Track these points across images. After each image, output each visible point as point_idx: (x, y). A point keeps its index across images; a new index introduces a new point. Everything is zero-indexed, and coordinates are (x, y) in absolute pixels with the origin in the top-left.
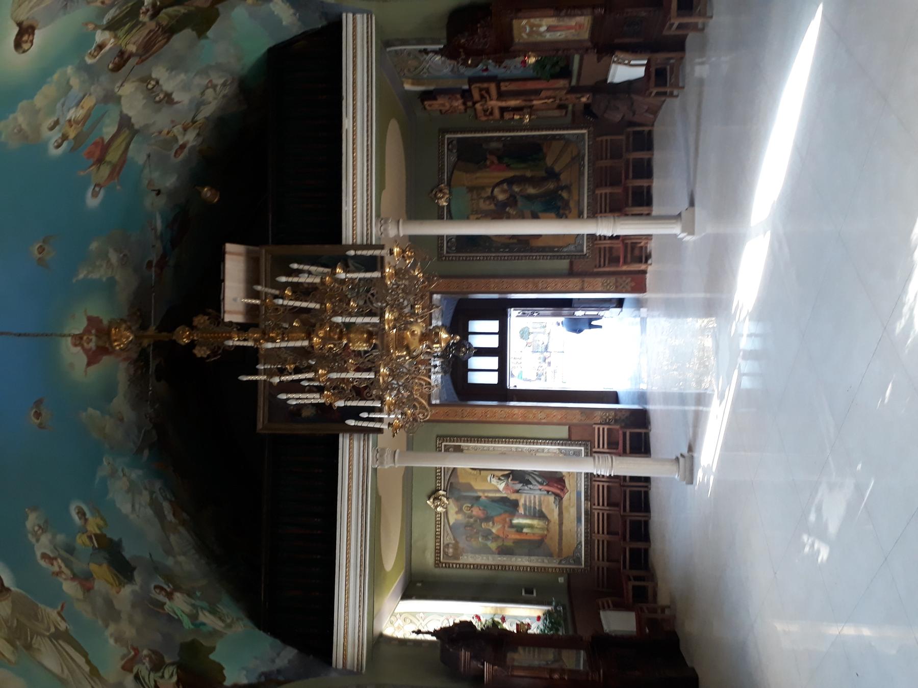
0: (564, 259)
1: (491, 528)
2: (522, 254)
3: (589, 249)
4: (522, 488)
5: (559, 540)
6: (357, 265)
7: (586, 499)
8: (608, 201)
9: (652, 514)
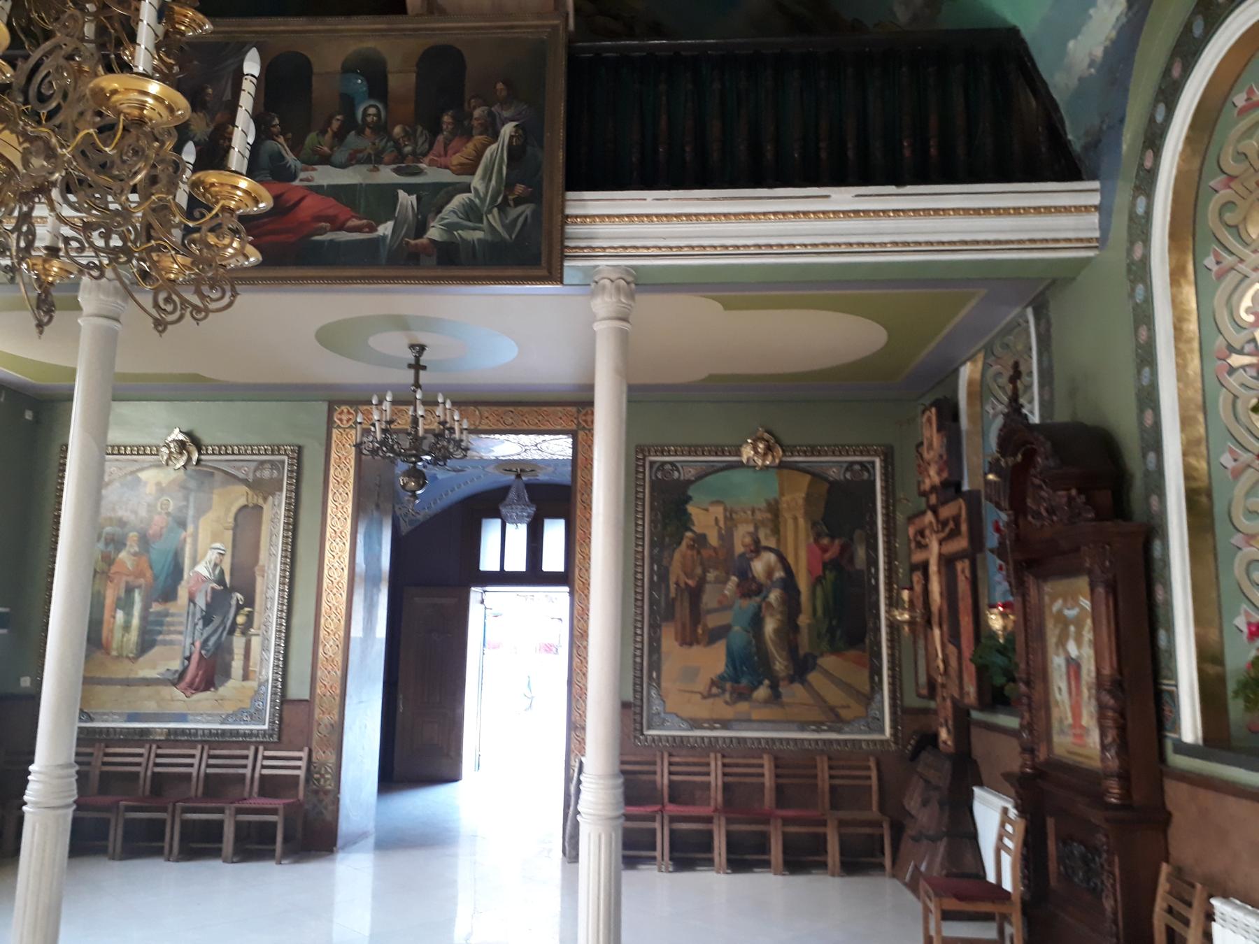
0: (635, 691)
1: (127, 548)
2: (646, 607)
3: (653, 740)
4: (198, 608)
5: (99, 678)
6: (521, 219)
7: (170, 732)
8: (748, 780)
9: (117, 864)
